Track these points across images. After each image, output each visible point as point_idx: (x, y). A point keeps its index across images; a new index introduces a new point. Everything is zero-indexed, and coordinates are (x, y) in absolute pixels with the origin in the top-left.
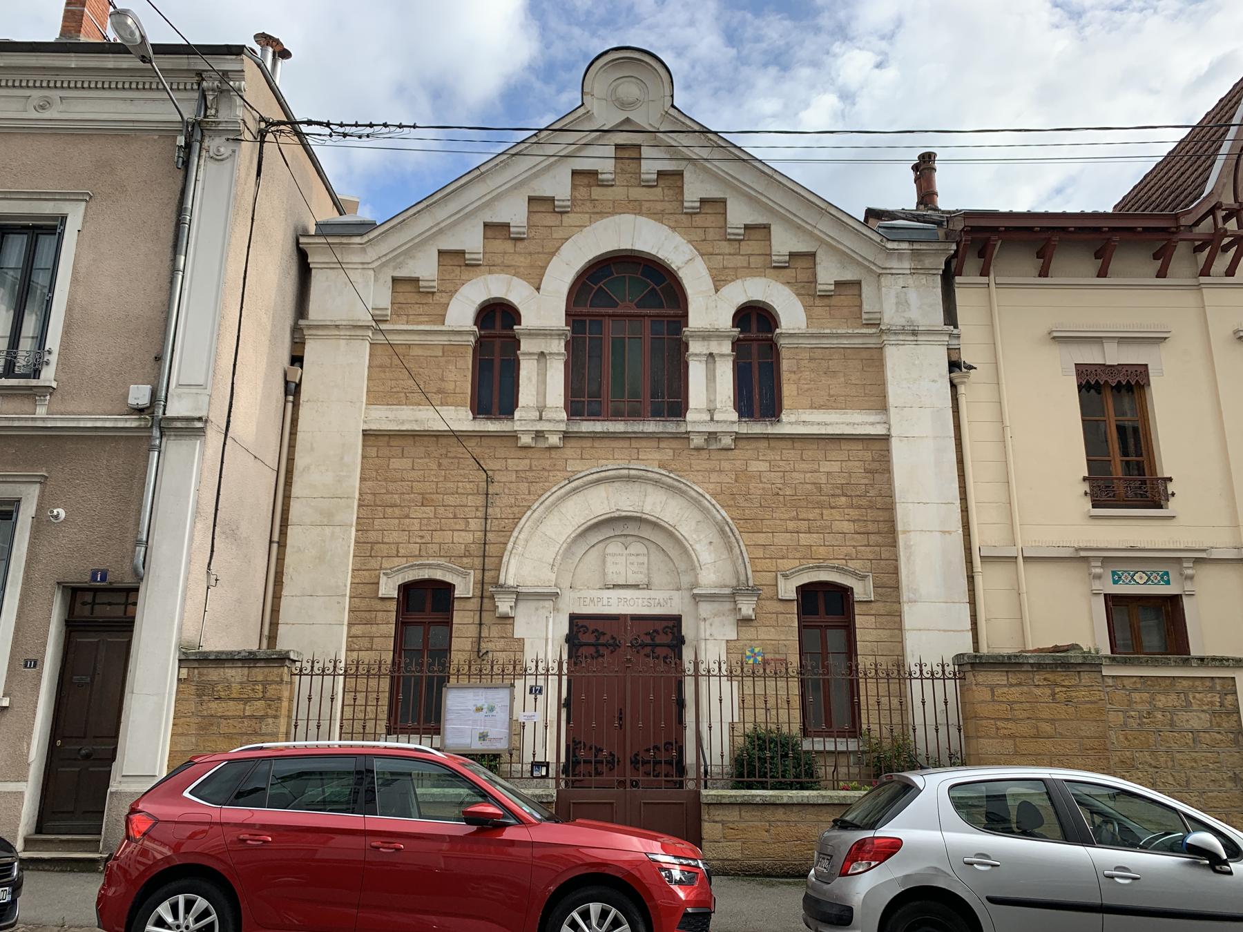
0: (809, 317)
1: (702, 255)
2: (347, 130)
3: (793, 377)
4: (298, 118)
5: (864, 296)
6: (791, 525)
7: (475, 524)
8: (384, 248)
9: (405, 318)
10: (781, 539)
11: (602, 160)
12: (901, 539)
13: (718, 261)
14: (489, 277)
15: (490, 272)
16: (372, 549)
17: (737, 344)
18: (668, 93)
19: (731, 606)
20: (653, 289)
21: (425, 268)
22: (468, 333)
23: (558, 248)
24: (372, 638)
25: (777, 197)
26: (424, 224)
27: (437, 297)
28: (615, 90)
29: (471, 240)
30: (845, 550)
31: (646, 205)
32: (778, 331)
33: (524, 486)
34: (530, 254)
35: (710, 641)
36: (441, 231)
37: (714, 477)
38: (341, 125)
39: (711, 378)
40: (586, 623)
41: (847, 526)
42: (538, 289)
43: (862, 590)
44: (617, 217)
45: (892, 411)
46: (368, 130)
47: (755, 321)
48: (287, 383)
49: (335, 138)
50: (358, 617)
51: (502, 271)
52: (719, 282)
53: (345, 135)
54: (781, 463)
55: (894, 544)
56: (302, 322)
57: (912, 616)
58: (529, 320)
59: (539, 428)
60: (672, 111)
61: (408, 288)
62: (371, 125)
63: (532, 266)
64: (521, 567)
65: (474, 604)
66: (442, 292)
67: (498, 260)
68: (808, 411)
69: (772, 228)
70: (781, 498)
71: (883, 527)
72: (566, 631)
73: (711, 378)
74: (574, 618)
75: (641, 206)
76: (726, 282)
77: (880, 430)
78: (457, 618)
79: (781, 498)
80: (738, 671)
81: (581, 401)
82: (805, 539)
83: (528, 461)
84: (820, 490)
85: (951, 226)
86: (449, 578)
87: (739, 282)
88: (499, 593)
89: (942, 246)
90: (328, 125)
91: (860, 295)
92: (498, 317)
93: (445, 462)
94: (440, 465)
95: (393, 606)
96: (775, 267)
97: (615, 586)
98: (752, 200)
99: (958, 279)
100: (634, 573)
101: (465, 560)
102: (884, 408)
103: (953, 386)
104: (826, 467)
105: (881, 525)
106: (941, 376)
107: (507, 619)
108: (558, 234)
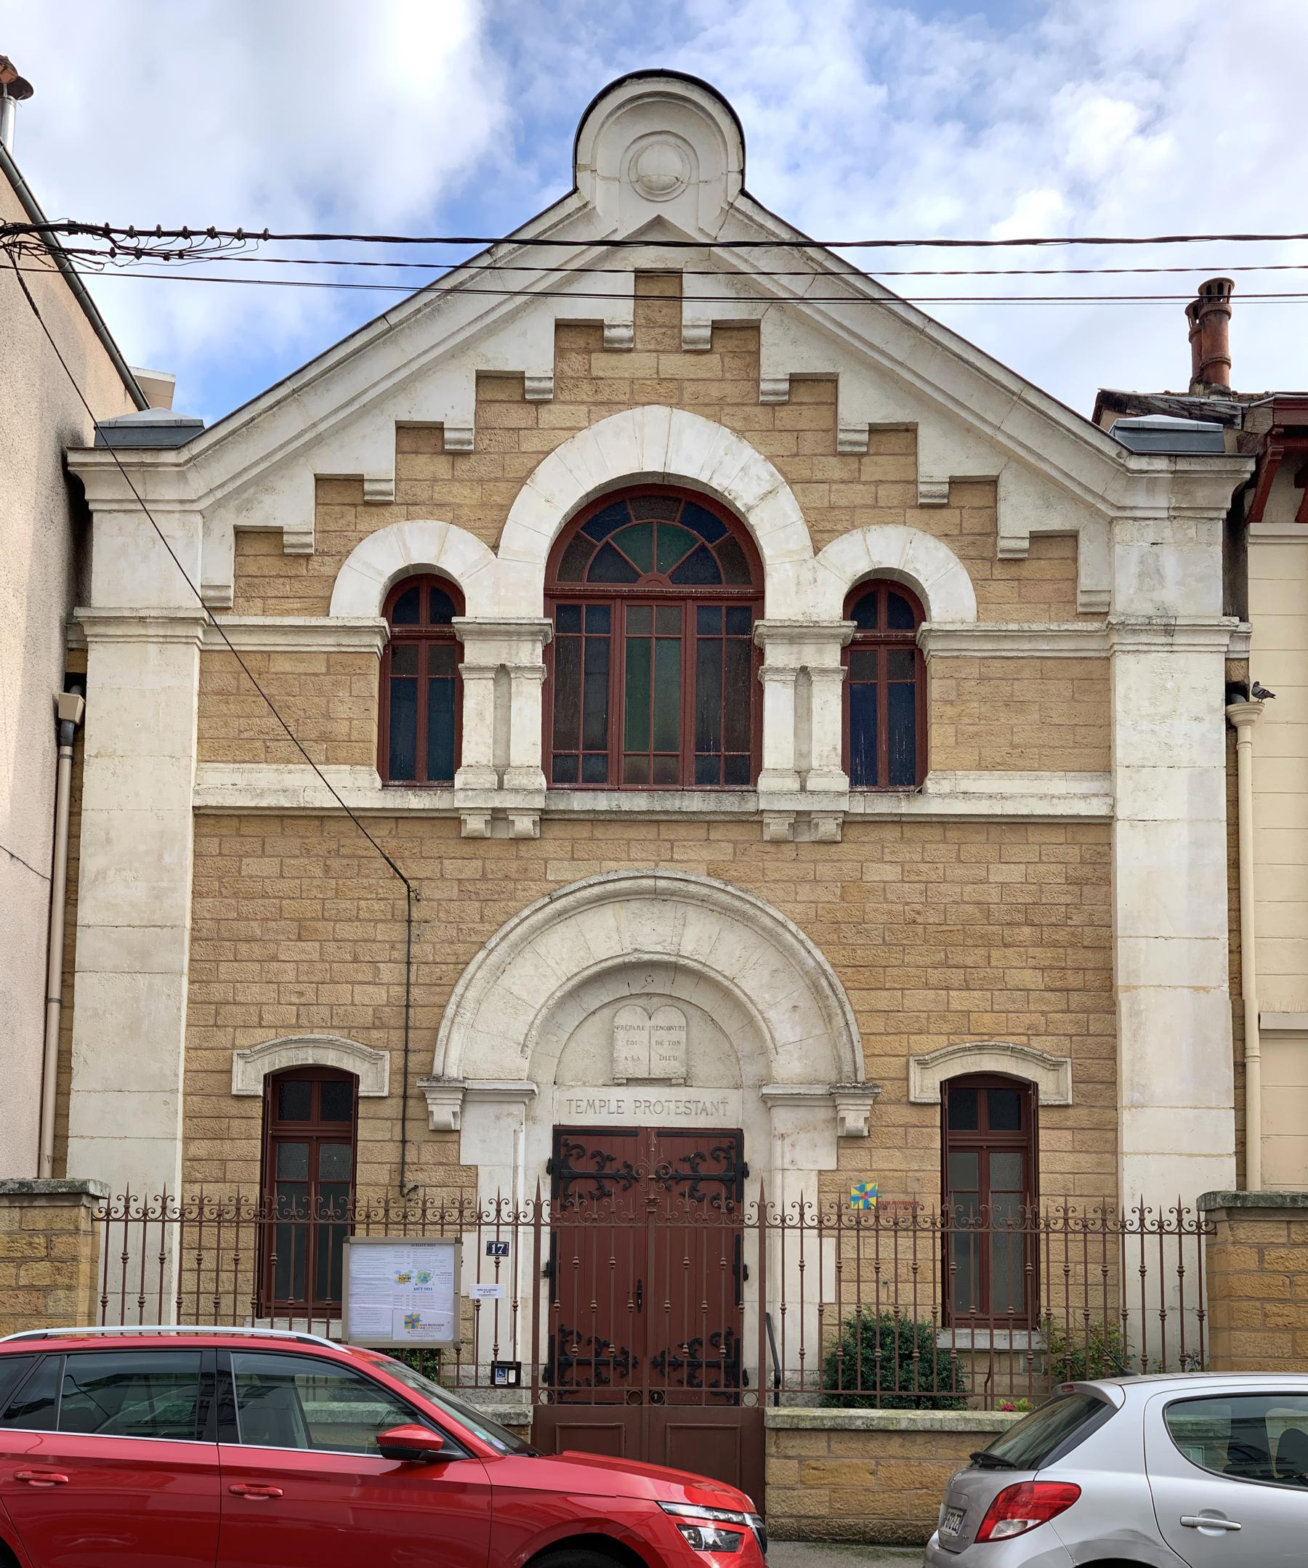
0: (982, 600)
1: (791, 483)
2: (143, 242)
3: (950, 711)
4: (53, 215)
5: (1081, 559)
6: (935, 976)
7: (391, 973)
8: (219, 471)
10: (919, 999)
11: (609, 300)
13: (818, 495)
14: (407, 526)
15: (409, 517)
16: (217, 1013)
17: (850, 651)
18: (735, 167)
20: (703, 548)
21: (292, 508)
23: (531, 471)
25: (931, 370)
26: (289, 425)
27: (315, 564)
29: (374, 456)
30: (1027, 1019)
31: (690, 388)
34: (481, 481)
36: (319, 440)
37: (805, 892)
38: (131, 233)
41: (1030, 978)
42: (495, 548)
43: (1052, 1087)
46: (181, 243)
47: (884, 604)
48: (59, 722)
49: (121, 259)
50: (200, 1125)
53: (139, 253)
54: (923, 867)
55: (1111, 1009)
57: (1135, 1131)
58: (478, 607)
59: (497, 804)
61: (262, 547)
62: (186, 234)
63: (483, 505)
66: (323, 554)
68: (973, 774)
69: (921, 431)
71: (1090, 981)
72: (548, 1154)
73: (803, 713)
74: (562, 1134)
75: (681, 389)
76: (834, 533)
77: (1096, 808)
79: (920, 929)
83: (480, 863)
86: (348, 1064)
87: (857, 535)
90: (106, 232)
91: (1075, 560)
93: (335, 863)
94: (327, 869)
96: (923, 506)
97: (631, 1081)
100: (662, 1058)
101: (375, 1034)
102: (1105, 768)
103: (1231, 728)
104: (1000, 873)
105: (1090, 976)
106: (1212, 710)
108: (531, 443)
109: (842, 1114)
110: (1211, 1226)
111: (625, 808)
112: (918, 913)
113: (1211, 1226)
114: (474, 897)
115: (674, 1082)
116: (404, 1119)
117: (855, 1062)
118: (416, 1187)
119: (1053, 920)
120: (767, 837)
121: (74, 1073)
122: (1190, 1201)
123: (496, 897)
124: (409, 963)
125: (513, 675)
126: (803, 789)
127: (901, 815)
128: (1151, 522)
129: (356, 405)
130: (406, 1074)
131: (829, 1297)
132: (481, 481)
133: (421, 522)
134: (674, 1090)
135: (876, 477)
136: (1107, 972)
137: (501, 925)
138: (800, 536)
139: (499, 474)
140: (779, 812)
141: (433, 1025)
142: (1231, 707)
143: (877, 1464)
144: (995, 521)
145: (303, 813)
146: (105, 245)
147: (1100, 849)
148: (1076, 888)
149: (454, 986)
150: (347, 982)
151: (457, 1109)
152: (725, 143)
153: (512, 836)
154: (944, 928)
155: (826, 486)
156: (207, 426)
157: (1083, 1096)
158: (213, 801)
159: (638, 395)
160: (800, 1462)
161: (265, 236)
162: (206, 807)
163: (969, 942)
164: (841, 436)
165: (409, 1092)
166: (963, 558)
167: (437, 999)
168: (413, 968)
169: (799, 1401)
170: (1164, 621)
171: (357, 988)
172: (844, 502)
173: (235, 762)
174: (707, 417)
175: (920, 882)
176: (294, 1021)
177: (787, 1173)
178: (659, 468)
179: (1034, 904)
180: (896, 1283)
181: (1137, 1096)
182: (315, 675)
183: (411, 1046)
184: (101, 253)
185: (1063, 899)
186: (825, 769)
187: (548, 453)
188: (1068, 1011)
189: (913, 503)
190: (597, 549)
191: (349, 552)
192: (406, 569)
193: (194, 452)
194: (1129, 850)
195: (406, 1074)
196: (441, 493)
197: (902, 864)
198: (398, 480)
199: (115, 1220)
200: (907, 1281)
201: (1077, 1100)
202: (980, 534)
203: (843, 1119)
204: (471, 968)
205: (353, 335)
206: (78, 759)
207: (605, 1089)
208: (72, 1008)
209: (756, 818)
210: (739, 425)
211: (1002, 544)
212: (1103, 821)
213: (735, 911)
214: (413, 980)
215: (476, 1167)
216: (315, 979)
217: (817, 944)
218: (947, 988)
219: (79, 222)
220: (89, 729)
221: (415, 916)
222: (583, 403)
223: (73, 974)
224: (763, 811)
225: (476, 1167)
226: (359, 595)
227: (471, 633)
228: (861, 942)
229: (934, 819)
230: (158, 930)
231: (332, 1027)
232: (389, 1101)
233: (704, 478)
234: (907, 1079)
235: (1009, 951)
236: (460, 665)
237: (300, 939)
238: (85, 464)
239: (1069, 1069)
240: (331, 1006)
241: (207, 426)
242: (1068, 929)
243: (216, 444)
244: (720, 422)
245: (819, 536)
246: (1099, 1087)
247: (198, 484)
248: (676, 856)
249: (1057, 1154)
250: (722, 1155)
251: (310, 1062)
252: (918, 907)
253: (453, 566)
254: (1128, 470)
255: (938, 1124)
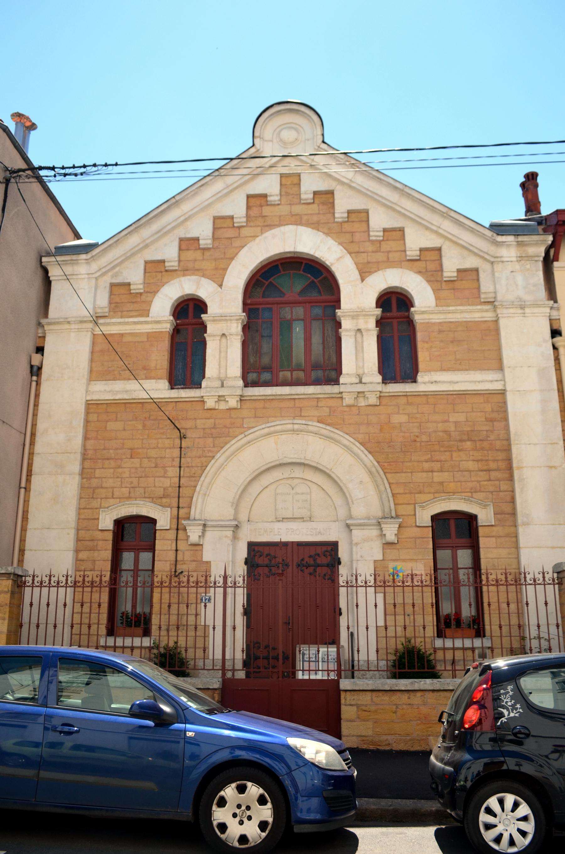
0: (437, 298)
1: (350, 253)
2: (67, 171)
3: (426, 345)
4: (36, 164)
5: (481, 279)
6: (426, 466)
7: (173, 472)
8: (103, 261)
9: (119, 314)
10: (420, 477)
11: (269, 185)
12: (516, 473)
13: (363, 258)
14: (183, 279)
15: (184, 275)
16: (94, 492)
17: (379, 323)
18: (319, 133)
19: (378, 527)
20: (313, 282)
21: (135, 275)
22: (166, 322)
23: (237, 254)
24: (94, 561)
25: (408, 205)
26: (134, 240)
27: (143, 297)
28: (279, 134)
29: (169, 252)
30: (470, 485)
31: (305, 218)
32: (412, 309)
33: (209, 441)
34: (215, 260)
35: (360, 558)
36: (147, 246)
37: (363, 429)
38: (63, 168)
39: (359, 349)
40: (261, 549)
41: (471, 465)
42: (221, 286)
43: (485, 516)
44: (282, 228)
45: (506, 370)
46: (82, 170)
47: (395, 304)
48: (32, 367)
49: (58, 178)
50: (82, 544)
51: (193, 274)
52: (364, 272)
53: (65, 175)
54: (418, 416)
55: (511, 478)
56: (44, 321)
57: (526, 536)
58: (213, 309)
59: (220, 394)
60: (324, 146)
61: (122, 290)
62: (85, 166)
63: (216, 269)
64: (213, 498)
65: (172, 535)
66: (147, 292)
67: (190, 265)
68: (438, 373)
69: (407, 231)
70: (418, 444)
71: (502, 465)
72: (245, 555)
73: (359, 349)
74: (252, 546)
75: (301, 218)
76: (371, 273)
77: (498, 386)
78: (159, 545)
79: (418, 444)
80: (383, 582)
81: (256, 371)
82: (437, 477)
83: (213, 420)
84: (450, 435)
85: (548, 223)
86: (152, 514)
87: (380, 272)
88: (189, 525)
89: (541, 237)
90: (53, 168)
91: (478, 280)
92: (190, 312)
93: (148, 423)
94: (144, 426)
95: (110, 536)
96: (409, 260)
97: (284, 519)
98: (390, 207)
99: (556, 264)
100: (299, 508)
101: (164, 500)
102: (501, 368)
103: (555, 348)
104: (454, 418)
105: (500, 463)
106: (545, 341)
107: (198, 546)
108: (237, 243)
109: (384, 533)
110: (560, 580)
111: (279, 393)
112: (417, 436)
113: (560, 580)
114: (210, 436)
115: (305, 519)
116: (177, 540)
117: (390, 507)
118: (182, 572)
119: (481, 438)
120: (344, 404)
121: (29, 520)
122: (549, 568)
123: (220, 436)
124: (180, 467)
125: (228, 338)
126: (361, 382)
127: (407, 392)
128: (509, 263)
129: (162, 232)
130: (178, 518)
131: (381, 623)
132: (215, 260)
133: (189, 277)
134: (305, 523)
135: (388, 249)
136: (509, 460)
137: (222, 448)
138: (356, 274)
139: (222, 256)
140: (349, 392)
141: (191, 495)
142: (555, 339)
143: (397, 708)
144: (441, 265)
145: (135, 401)
146: (52, 173)
147: (501, 405)
148: (491, 423)
149: (200, 477)
150: (152, 477)
151: (200, 534)
152: (315, 125)
153: (227, 408)
154: (430, 443)
155: (366, 254)
156: (100, 243)
157: (500, 521)
158: (95, 397)
159: (282, 222)
160: (357, 707)
161: (116, 164)
162: (92, 400)
163: (442, 449)
164: (371, 233)
165: (179, 527)
166: (428, 281)
167: (193, 484)
168: (182, 469)
169: (368, 676)
170: (520, 303)
171: (157, 479)
172: (374, 260)
173: (106, 380)
174: (313, 228)
175: (417, 422)
176: (128, 495)
177: (359, 562)
178: (292, 250)
179: (471, 431)
180: (414, 615)
181: (525, 519)
182: (142, 342)
183: (180, 506)
184: (50, 176)
185: (485, 428)
186: (371, 373)
187: (243, 247)
188: (490, 480)
189: (405, 259)
190: (266, 285)
191: (158, 291)
192: (183, 296)
193: (93, 254)
194: (515, 406)
195: (178, 518)
196: (197, 265)
197: (408, 414)
198: (180, 261)
199: (28, 586)
200: (420, 614)
201: (497, 523)
202: (435, 271)
203: (385, 535)
204: (208, 468)
205: (161, 205)
206: (39, 382)
207: (272, 524)
208: (30, 491)
209: (339, 396)
210: (326, 231)
211: (445, 274)
212: (500, 392)
213: (332, 438)
214: (182, 475)
215: (210, 562)
216: (137, 476)
217: (370, 452)
218: (432, 471)
219: (42, 166)
220: (44, 370)
221: (183, 446)
222: (259, 226)
223: (31, 476)
224: (342, 393)
225: (210, 562)
226: (162, 308)
227: (210, 321)
228: (391, 451)
229: (422, 394)
230: (69, 454)
231: (145, 497)
232: (170, 531)
233: (312, 253)
234: (415, 515)
235: (461, 453)
236: (205, 335)
237: (131, 457)
238: (49, 262)
239: (492, 508)
240: (145, 488)
241: (100, 243)
242: (488, 442)
243: (103, 250)
244: (318, 230)
245: (363, 275)
246: (507, 516)
247: (94, 266)
248: (303, 414)
249: (491, 552)
250: (328, 554)
251: (135, 514)
252: (417, 434)
253: (203, 294)
254: (497, 242)
255: (431, 536)
